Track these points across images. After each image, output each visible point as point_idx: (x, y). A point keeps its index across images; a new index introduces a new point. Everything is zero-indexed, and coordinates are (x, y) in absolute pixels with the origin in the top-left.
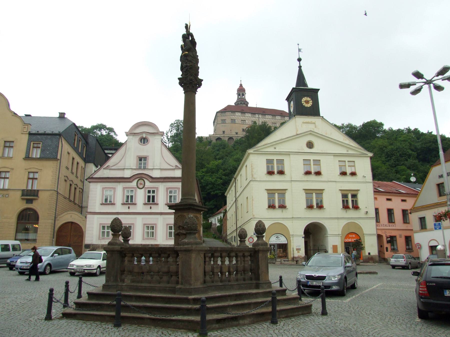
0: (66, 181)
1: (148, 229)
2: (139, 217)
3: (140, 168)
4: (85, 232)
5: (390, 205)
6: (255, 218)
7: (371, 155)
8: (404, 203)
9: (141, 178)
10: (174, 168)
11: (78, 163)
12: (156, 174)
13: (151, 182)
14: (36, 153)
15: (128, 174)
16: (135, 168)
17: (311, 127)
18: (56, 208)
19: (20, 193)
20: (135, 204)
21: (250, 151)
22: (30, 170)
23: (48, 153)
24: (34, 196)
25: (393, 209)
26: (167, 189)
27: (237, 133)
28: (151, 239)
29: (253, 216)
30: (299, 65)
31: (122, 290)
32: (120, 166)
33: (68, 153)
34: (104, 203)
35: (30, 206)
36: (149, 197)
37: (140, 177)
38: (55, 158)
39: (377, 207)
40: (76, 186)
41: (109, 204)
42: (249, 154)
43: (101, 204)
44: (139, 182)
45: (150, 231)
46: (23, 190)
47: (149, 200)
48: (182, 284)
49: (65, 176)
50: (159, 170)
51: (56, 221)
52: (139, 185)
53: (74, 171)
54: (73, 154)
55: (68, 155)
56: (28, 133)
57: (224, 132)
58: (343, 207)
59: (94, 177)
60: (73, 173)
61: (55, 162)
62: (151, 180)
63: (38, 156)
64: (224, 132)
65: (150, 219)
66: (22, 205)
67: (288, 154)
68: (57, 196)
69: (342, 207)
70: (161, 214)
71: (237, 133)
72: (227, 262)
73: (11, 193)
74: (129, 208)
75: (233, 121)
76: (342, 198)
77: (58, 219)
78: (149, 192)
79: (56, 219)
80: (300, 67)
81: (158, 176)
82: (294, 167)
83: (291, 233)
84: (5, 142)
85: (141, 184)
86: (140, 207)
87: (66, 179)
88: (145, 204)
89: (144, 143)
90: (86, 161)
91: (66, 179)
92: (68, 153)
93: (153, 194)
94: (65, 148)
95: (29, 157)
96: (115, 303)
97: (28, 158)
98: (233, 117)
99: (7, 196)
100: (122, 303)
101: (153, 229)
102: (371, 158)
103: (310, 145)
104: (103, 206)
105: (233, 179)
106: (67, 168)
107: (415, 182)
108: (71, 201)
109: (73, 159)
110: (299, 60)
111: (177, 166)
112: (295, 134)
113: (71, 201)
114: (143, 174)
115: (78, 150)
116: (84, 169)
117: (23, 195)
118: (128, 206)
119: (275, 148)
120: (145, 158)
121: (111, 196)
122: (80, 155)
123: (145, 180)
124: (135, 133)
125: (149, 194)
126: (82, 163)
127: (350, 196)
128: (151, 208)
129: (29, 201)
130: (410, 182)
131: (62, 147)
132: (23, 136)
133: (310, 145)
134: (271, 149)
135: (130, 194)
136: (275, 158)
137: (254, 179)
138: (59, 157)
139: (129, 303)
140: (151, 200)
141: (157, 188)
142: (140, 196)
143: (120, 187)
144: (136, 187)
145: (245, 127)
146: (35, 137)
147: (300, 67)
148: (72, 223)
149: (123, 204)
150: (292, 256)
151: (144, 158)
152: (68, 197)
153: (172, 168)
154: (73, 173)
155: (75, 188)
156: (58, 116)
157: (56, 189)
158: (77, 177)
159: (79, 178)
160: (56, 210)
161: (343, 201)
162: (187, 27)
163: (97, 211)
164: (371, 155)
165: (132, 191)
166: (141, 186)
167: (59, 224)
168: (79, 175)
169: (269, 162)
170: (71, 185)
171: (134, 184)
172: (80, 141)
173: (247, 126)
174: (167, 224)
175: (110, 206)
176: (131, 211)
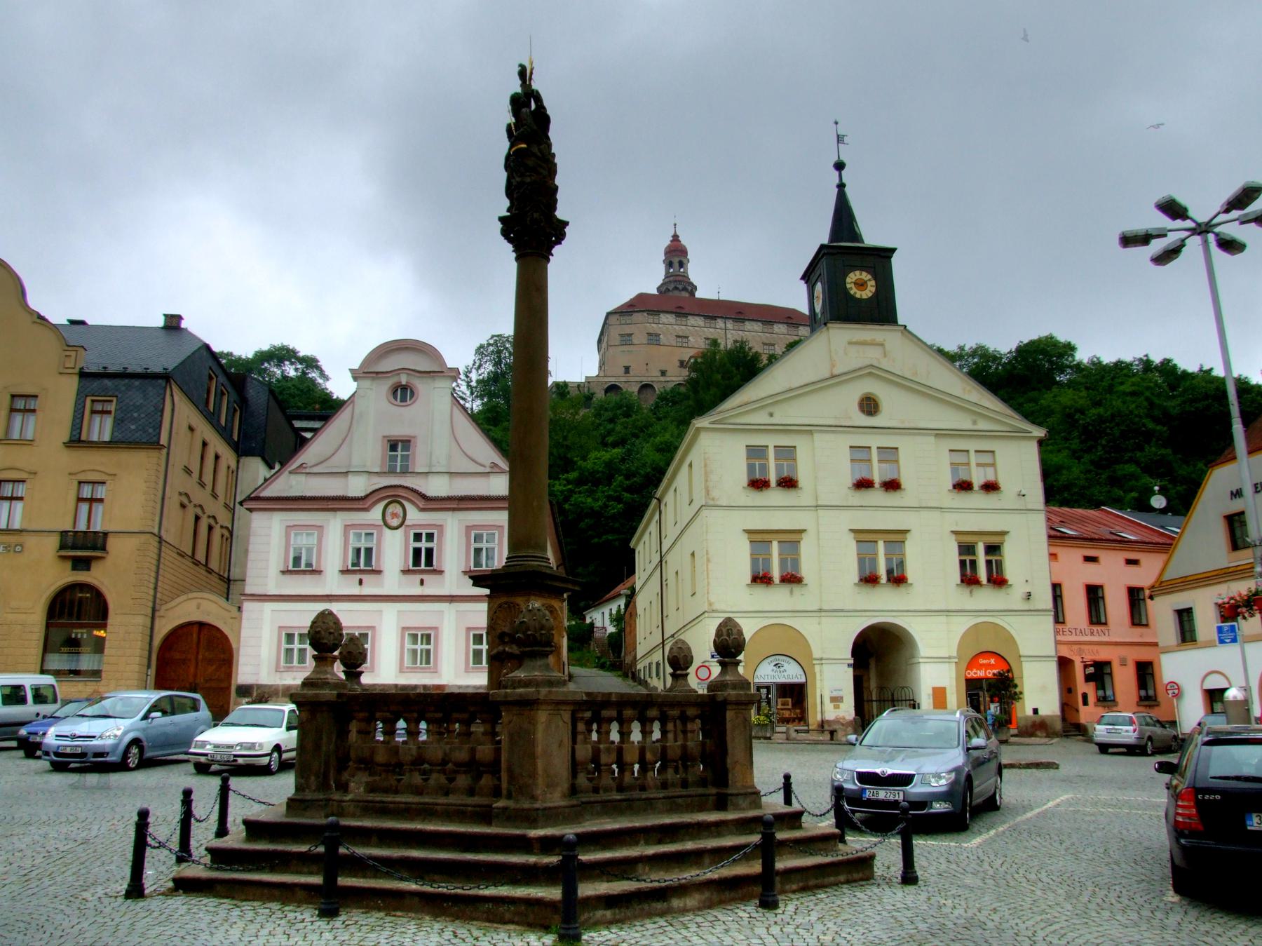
0: (183, 506)
1: (415, 642)
2: (390, 610)
3: (392, 471)
4: (238, 649)
5: (1093, 574)
6: (713, 611)
7: (1040, 432)
8: (1133, 568)
9: (395, 500)
10: (488, 470)
11: (217, 457)
12: (437, 487)
14: (101, 428)
15: (357, 486)
16: (377, 470)
17: (872, 356)
21: (700, 422)
23: (133, 427)
24: (94, 548)
25: (1101, 587)
27: (663, 373)
29: (710, 604)
30: (837, 181)
31: (341, 814)
32: (337, 463)
34: (291, 568)
35: (82, 577)
36: (417, 552)
38: (152, 443)
39: (1056, 581)
41: (304, 572)
42: (698, 430)
43: (283, 572)
44: (391, 509)
45: (419, 647)
47: (417, 561)
48: (509, 796)
49: (180, 494)
52: (388, 518)
53: (208, 478)
56: (77, 371)
57: (627, 369)
58: (962, 581)
59: (262, 495)
60: (202, 485)
62: (422, 504)
63: (107, 438)
64: (627, 369)
65: (421, 615)
66: (66, 576)
67: (807, 430)
69: (959, 581)
70: (452, 599)
71: (663, 373)
73: (30, 541)
74: (361, 582)
75: (653, 338)
76: (960, 554)
77: (161, 613)
78: (418, 537)
79: (157, 614)
80: (841, 186)
81: (443, 494)
82: (825, 465)
83: (816, 653)
85: (394, 515)
86: (392, 580)
87: (185, 501)
88: (406, 572)
89: (404, 399)
91: (185, 501)
92: (191, 429)
93: (429, 545)
94: (181, 414)
95: (79, 441)
96: (321, 849)
97: (76, 441)
98: (654, 328)
100: (342, 850)
101: (428, 643)
102: (1041, 442)
103: (869, 406)
104: (288, 577)
105: (654, 502)
106: (188, 471)
107: (1163, 511)
108: (197, 563)
109: (205, 444)
110: (840, 166)
111: (495, 465)
112: (827, 375)
113: (197, 563)
114: (400, 486)
115: (219, 421)
116: (234, 474)
118: (358, 577)
119: (771, 415)
120: (407, 443)
121: (309, 550)
122: (224, 433)
123: (405, 503)
125: (418, 545)
127: (980, 549)
129: (82, 564)
130: (1152, 509)
131: (173, 410)
133: (869, 406)
134: (760, 418)
135: (363, 544)
136: (771, 441)
137: (711, 503)
138: (164, 441)
139: (361, 851)
141: (440, 528)
142: (393, 550)
143: (334, 525)
144: (381, 523)
145: (686, 354)
146: (96, 384)
147: (841, 186)
148: (201, 625)
149: (345, 572)
150: (819, 718)
152: (190, 553)
153: (481, 469)
155: (210, 528)
157: (156, 531)
158: (215, 496)
160: (155, 588)
161: (962, 563)
162: (523, 74)
164: (1040, 432)
165: (369, 535)
166: (395, 522)
167: (164, 628)
168: (220, 489)
169: (756, 453)
170: (197, 518)
171: (376, 514)
173: (692, 352)
174: (469, 629)
175: (308, 577)
176: (366, 590)
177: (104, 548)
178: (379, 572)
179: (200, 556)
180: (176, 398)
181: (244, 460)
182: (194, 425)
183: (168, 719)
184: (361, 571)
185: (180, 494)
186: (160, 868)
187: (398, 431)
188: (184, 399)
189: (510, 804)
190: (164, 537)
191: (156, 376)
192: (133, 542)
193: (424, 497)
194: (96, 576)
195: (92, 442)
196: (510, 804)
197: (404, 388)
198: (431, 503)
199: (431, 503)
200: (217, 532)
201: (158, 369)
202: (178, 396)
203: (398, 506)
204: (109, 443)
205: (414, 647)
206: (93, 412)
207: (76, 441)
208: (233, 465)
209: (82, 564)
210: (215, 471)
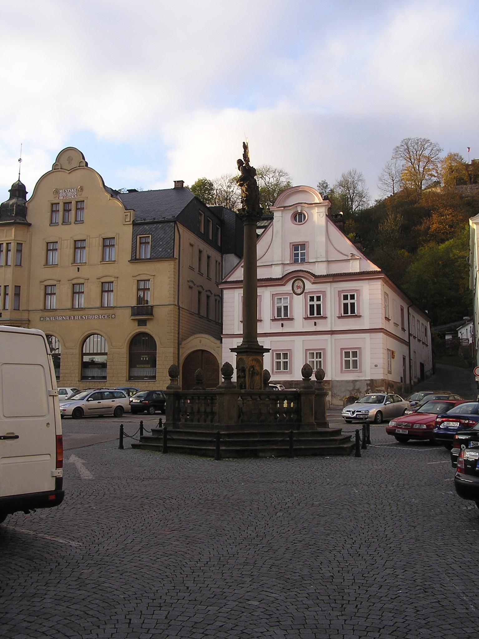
0: (190, 287)
3: (296, 261)
9: (298, 279)
11: (209, 257)
12: (321, 270)
13: (313, 283)
14: (146, 252)
16: (288, 262)
18: (179, 331)
19: (129, 312)
20: (292, 319)
22: (139, 278)
23: (160, 250)
24: (147, 314)
26: (340, 292)
28: (353, 372)
31: (179, 428)
33: (191, 245)
35: (143, 329)
37: (295, 277)
38: (170, 257)
40: (209, 293)
44: (296, 284)
45: (315, 360)
46: (133, 308)
47: (312, 313)
48: (219, 422)
49: (188, 281)
50: (325, 264)
51: (181, 349)
52: (295, 289)
53: (204, 270)
54: (200, 244)
55: (191, 248)
56: (131, 222)
60: (202, 275)
61: (172, 263)
63: (149, 257)
66: (134, 329)
68: (179, 312)
72: (285, 405)
73: (118, 312)
74: (282, 325)
77: (183, 345)
78: (312, 299)
79: (180, 346)
84: (104, 239)
85: (298, 287)
87: (192, 285)
88: (307, 318)
89: (300, 221)
90: (223, 250)
91: (192, 285)
92: (191, 245)
94: (186, 237)
95: (136, 259)
97: (135, 259)
99: (113, 316)
106: (191, 268)
108: (202, 317)
109: (200, 252)
111: (353, 255)
113: (202, 317)
114: (301, 271)
115: (208, 237)
116: (220, 265)
117: (133, 314)
118: (399, 323)
120: (303, 246)
122: (212, 244)
124: (284, 207)
126: (215, 255)
128: (315, 324)
129: (142, 323)
131: (180, 238)
132: (126, 227)
135: (282, 305)
138: (176, 256)
139: (175, 437)
140: (315, 312)
141: (324, 293)
142: (299, 307)
146: (141, 228)
148: (203, 351)
149: (274, 320)
151: (300, 245)
152: (197, 313)
153: (346, 258)
154: (202, 275)
155: (208, 297)
156: (173, 187)
157: (176, 303)
158: (209, 279)
159: (213, 279)
160: (178, 333)
162: (245, 147)
163: (367, 335)
166: (299, 291)
167: (184, 353)
168: (212, 275)
170: (200, 293)
171: (288, 288)
172: (209, 221)
174: (342, 349)
176: (319, 328)
177: (152, 314)
178: (292, 319)
179: (203, 313)
180: (181, 231)
181: (224, 256)
182: (192, 243)
183: (392, 404)
184: (282, 319)
185: (188, 281)
186: (127, 442)
187: (298, 239)
188: (186, 230)
189: (219, 424)
190: (181, 306)
191: (169, 221)
192: (165, 310)
193: (314, 275)
194: (148, 329)
195: (143, 259)
196: (219, 424)
197: (300, 214)
198: (318, 279)
199: (318, 279)
200: (212, 298)
201: (170, 217)
202: (181, 228)
203: (300, 282)
204: (150, 259)
205: (313, 360)
206: (141, 243)
207: (135, 259)
208: (219, 260)
209: (142, 323)
210: (208, 266)
